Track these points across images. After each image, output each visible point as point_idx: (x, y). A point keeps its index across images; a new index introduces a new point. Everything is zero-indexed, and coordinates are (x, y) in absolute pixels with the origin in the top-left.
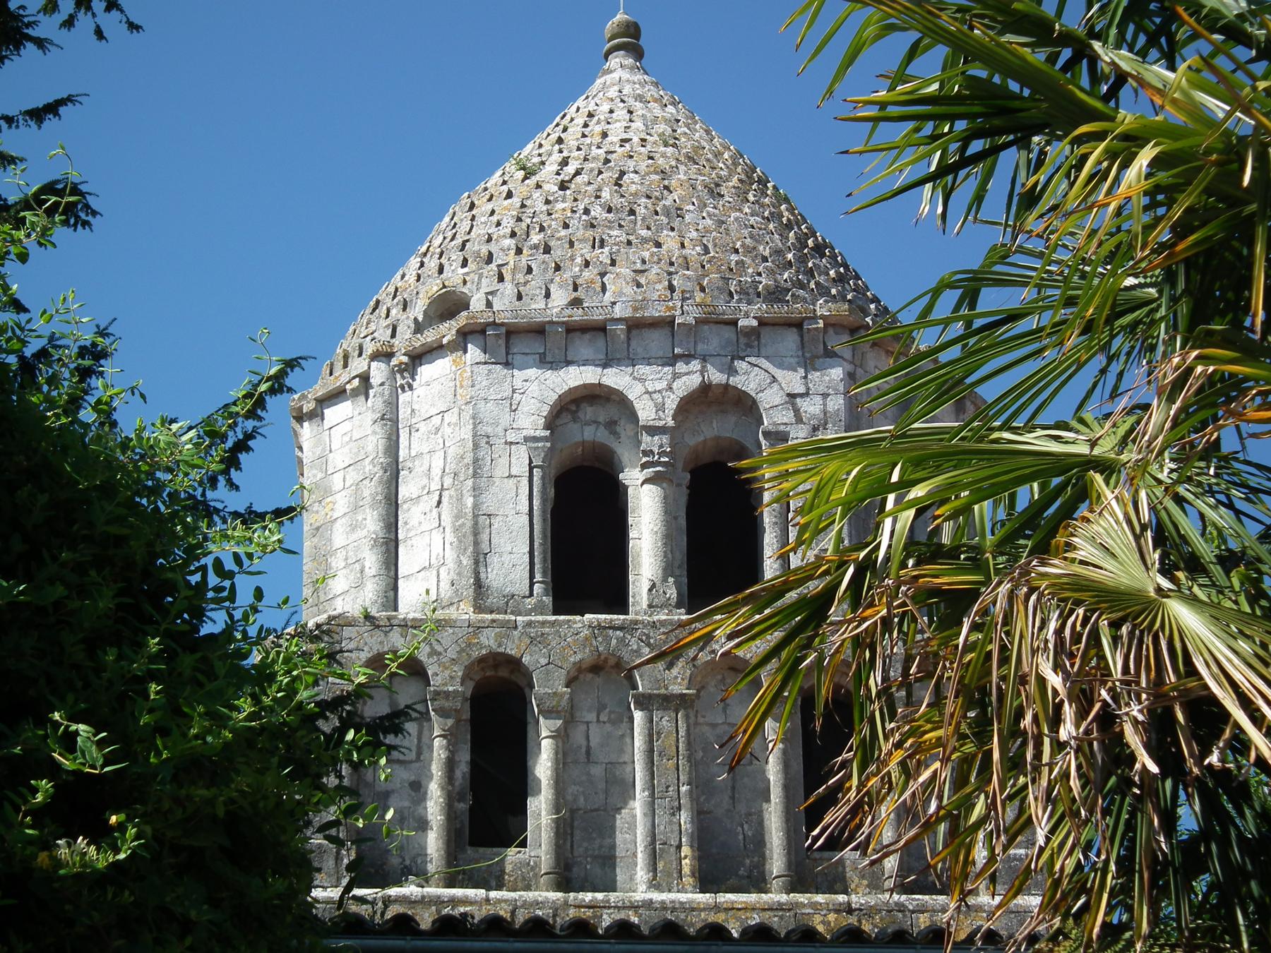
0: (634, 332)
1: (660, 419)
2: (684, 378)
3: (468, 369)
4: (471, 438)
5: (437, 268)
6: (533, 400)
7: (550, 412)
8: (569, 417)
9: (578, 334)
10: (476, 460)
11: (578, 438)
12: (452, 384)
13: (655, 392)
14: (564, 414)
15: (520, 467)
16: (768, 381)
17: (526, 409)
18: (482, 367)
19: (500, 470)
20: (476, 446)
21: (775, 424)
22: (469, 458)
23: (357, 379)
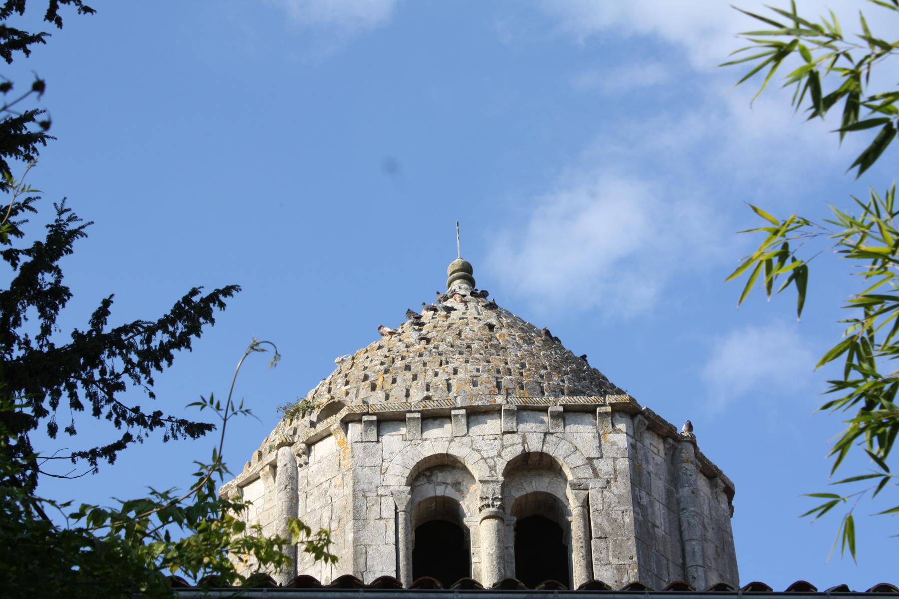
0: (472, 418)
1: (493, 476)
2: (510, 449)
3: (349, 447)
4: (351, 493)
5: (327, 389)
6: (397, 466)
7: (411, 474)
8: (425, 480)
9: (431, 421)
10: (355, 508)
11: (432, 494)
12: (337, 459)
13: (489, 458)
14: (421, 478)
15: (389, 513)
16: (572, 450)
17: (391, 473)
18: (358, 444)
19: (374, 513)
20: (355, 497)
21: (579, 479)
22: (350, 507)
23: (268, 467)
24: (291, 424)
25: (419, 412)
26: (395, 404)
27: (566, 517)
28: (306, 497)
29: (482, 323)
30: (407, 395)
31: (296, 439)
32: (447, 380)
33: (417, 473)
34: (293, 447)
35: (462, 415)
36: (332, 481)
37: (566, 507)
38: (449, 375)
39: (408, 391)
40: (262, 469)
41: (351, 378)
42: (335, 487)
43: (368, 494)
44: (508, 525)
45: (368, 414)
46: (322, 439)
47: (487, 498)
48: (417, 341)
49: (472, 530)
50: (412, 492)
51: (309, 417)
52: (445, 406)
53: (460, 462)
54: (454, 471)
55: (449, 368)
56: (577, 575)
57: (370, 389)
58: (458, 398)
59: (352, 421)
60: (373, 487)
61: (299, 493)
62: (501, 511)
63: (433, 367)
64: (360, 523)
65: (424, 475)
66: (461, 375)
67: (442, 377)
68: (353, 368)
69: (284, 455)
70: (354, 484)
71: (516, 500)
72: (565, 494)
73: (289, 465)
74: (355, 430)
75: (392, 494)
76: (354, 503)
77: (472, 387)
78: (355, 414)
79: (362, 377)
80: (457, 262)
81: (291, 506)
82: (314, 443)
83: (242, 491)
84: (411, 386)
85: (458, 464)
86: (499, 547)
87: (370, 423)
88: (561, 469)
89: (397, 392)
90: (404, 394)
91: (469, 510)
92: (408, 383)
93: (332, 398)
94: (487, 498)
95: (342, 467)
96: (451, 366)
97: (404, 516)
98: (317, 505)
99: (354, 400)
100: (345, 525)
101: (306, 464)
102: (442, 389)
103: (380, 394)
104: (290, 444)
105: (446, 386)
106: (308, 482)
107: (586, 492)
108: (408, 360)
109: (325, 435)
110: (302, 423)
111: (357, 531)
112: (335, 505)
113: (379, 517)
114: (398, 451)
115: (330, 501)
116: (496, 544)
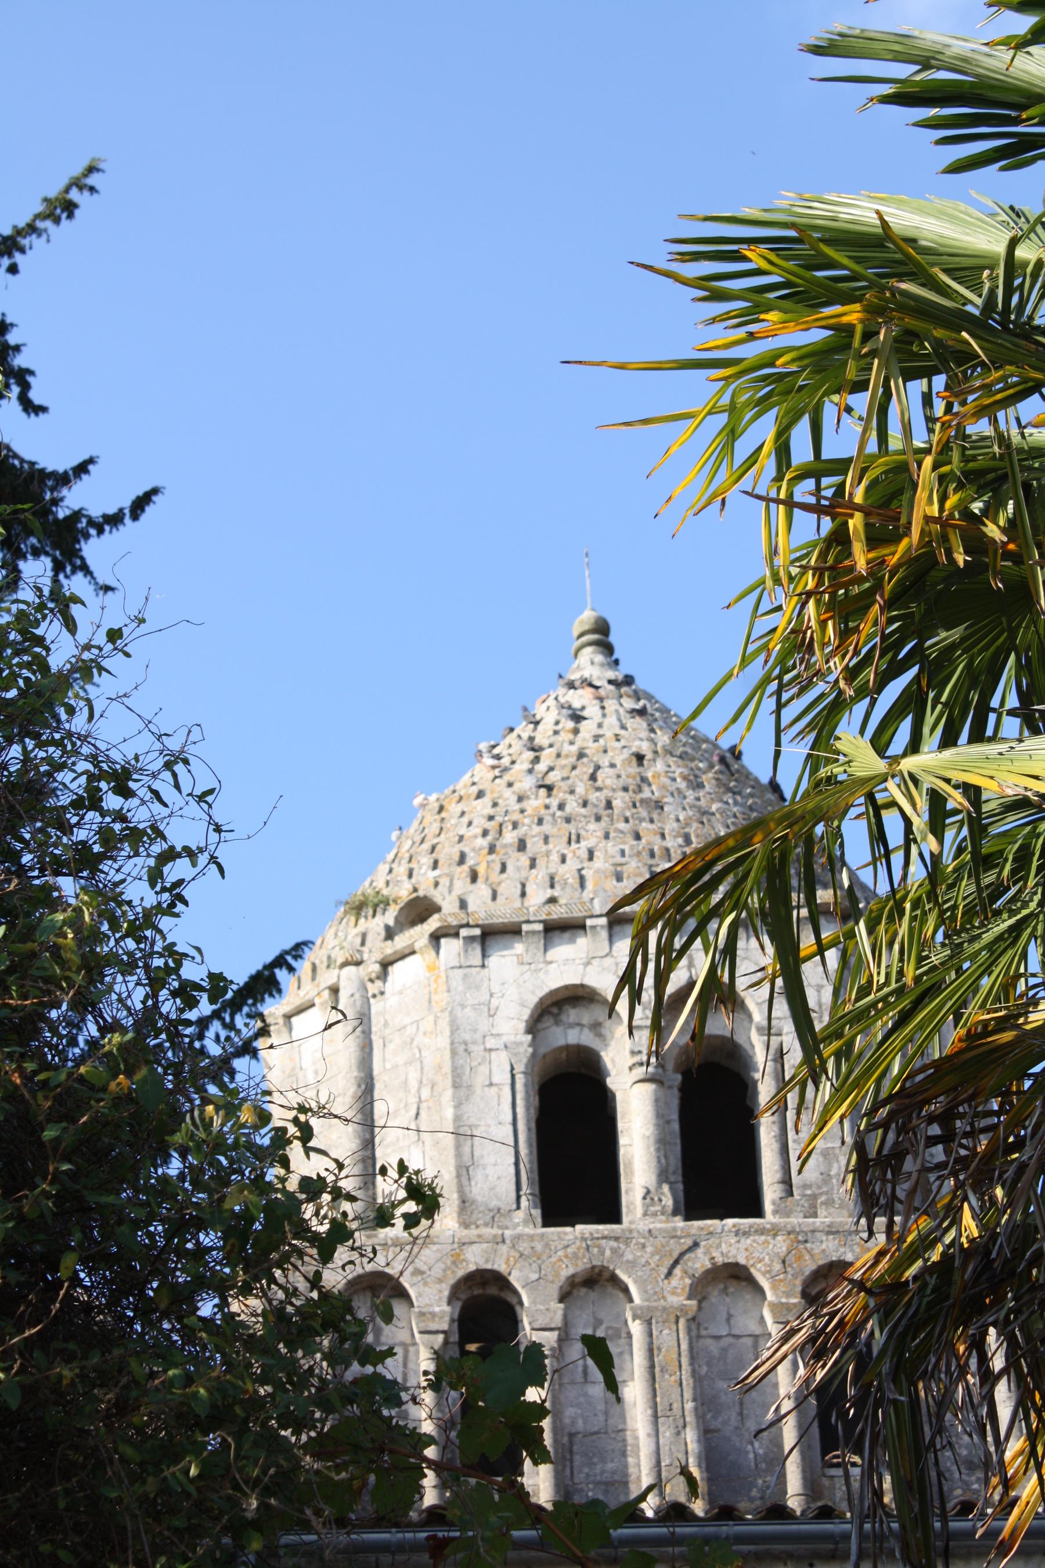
3: (443, 975)
4: (448, 1047)
7: (532, 1016)
8: (552, 1020)
9: (557, 933)
10: (454, 1069)
11: (561, 1042)
12: (426, 991)
14: (546, 1018)
18: (456, 971)
19: (480, 1079)
20: (454, 1053)
22: (447, 1068)
24: (356, 924)
25: (540, 922)
26: (503, 912)
27: (752, 1074)
28: (384, 1045)
29: (626, 754)
30: (523, 894)
31: (366, 957)
32: (579, 870)
33: (539, 1011)
34: (361, 967)
35: (602, 927)
36: (421, 1024)
37: (751, 1057)
38: (582, 862)
39: (523, 886)
40: (319, 994)
41: (441, 855)
42: (425, 1033)
43: (471, 1048)
44: (670, 1087)
45: (467, 925)
46: (403, 957)
47: (640, 1052)
48: (534, 790)
49: (619, 1097)
50: (533, 1043)
51: (382, 917)
52: (577, 913)
53: (600, 995)
54: (593, 1006)
55: (581, 851)
56: (768, 1164)
57: (468, 880)
58: (596, 902)
59: (446, 935)
60: (478, 1036)
61: (374, 1037)
62: (660, 1070)
63: (558, 846)
64: (462, 1092)
65: (549, 1013)
66: (599, 863)
67: (572, 865)
68: (442, 835)
69: (349, 979)
70: (452, 1033)
71: (681, 1048)
72: (749, 1038)
73: (357, 996)
74: (450, 947)
75: (506, 1047)
76: (453, 1062)
77: (614, 882)
78: (449, 926)
79: (456, 857)
80: (587, 617)
81: (364, 1058)
82: (392, 963)
83: (290, 1023)
84: (527, 879)
85: (596, 997)
86: (658, 1126)
87: (470, 939)
88: (743, 1002)
89: (509, 888)
90: (519, 891)
91: (614, 1066)
92: (524, 873)
93: (415, 890)
94: (640, 1052)
95: (433, 1004)
96: (584, 844)
97: (523, 1080)
98: (401, 1059)
99: (447, 895)
100: (440, 1095)
101: (382, 993)
102: (572, 886)
103: (484, 891)
104: (358, 963)
105: (578, 880)
106: (386, 1022)
107: (779, 1038)
108: (522, 831)
109: (407, 952)
110: (376, 925)
111: (458, 1106)
112: (426, 1061)
113: (488, 1083)
114: (511, 981)
115: (418, 1055)
116: (653, 1121)
